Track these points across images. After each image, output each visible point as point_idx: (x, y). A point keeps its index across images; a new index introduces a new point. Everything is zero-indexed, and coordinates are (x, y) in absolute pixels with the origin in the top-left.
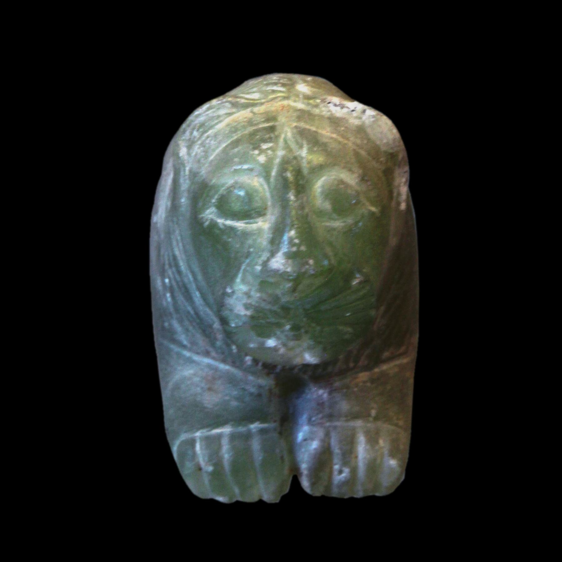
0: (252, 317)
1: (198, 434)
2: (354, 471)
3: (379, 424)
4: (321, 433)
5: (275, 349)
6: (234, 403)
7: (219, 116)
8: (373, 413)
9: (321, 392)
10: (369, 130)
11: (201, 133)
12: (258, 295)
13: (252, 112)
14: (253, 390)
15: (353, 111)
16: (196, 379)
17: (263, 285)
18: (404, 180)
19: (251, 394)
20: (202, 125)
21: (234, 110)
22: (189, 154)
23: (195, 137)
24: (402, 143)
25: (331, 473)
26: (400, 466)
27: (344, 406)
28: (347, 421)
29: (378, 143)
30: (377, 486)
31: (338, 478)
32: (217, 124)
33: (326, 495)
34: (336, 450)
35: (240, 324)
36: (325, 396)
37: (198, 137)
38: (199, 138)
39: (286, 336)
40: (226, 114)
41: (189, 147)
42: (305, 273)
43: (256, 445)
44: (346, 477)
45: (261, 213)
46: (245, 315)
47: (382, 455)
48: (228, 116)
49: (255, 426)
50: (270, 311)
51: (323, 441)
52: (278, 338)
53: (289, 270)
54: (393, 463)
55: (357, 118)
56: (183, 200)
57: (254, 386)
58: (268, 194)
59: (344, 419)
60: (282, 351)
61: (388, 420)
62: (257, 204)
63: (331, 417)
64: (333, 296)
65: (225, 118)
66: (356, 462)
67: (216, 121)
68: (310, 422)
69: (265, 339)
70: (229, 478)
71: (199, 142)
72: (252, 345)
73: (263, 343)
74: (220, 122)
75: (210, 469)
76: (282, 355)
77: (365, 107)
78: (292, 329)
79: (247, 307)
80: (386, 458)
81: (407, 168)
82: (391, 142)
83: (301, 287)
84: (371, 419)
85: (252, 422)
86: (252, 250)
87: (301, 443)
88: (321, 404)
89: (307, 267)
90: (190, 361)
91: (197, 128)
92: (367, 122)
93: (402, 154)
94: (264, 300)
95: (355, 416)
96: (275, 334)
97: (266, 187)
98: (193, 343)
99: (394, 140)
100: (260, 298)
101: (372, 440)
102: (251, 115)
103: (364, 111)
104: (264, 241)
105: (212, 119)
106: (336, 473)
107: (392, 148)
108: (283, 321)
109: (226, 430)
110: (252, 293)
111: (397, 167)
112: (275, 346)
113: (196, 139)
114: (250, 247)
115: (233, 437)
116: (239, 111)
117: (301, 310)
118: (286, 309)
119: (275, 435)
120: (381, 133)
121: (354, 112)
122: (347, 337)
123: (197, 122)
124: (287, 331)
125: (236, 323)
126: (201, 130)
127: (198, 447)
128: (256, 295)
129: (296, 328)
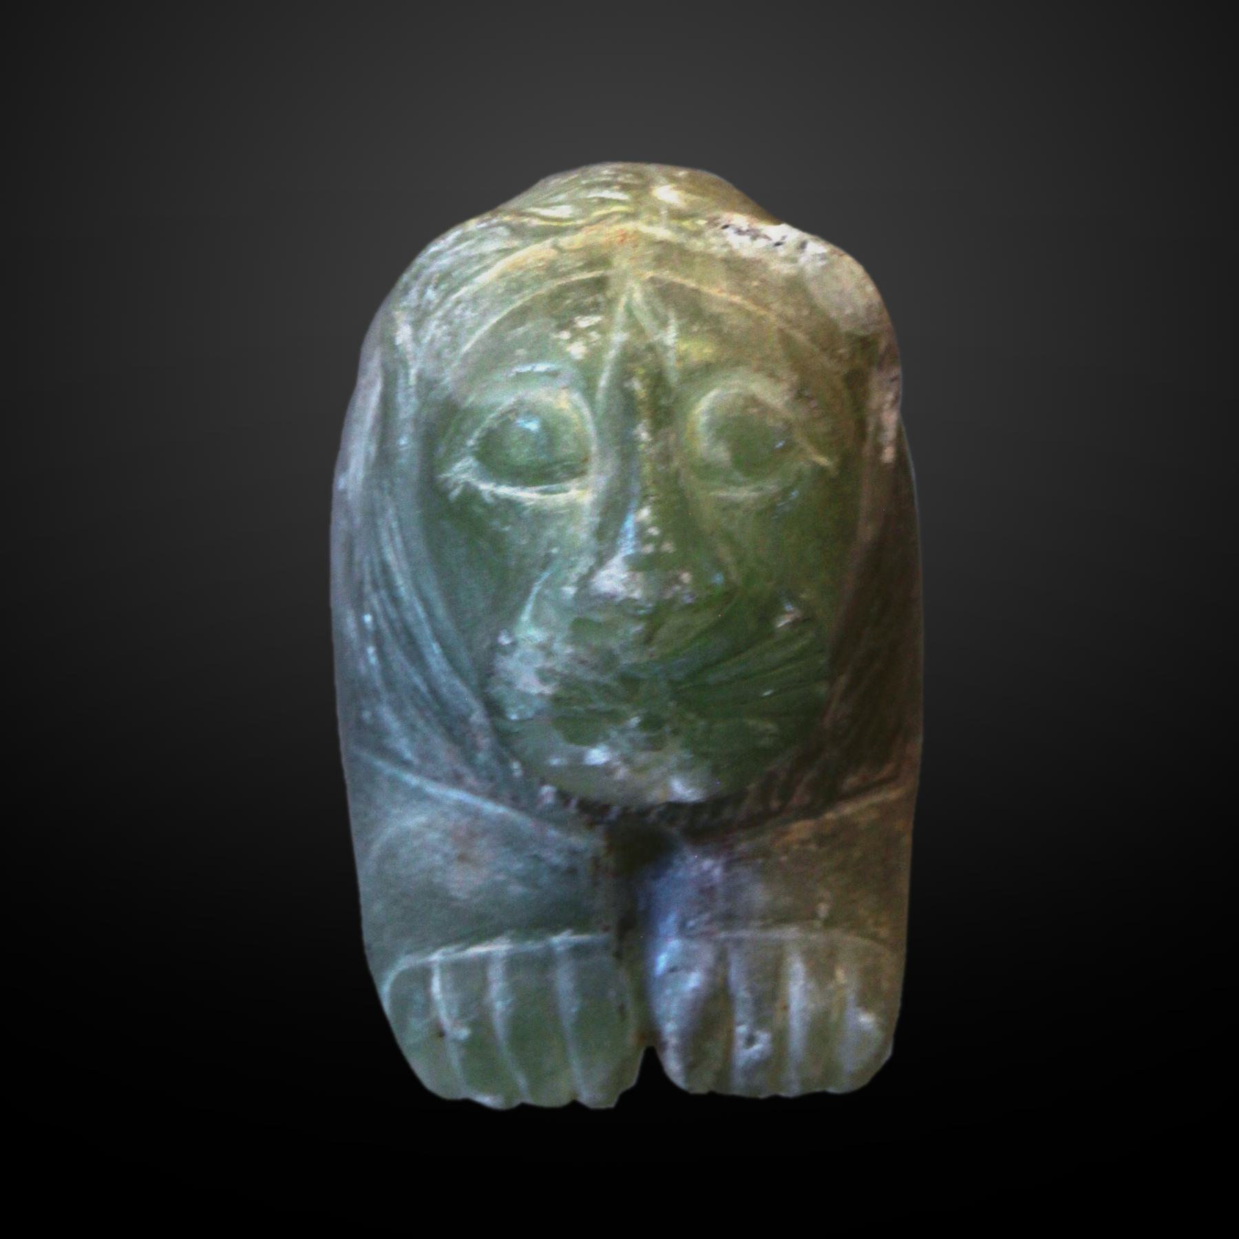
1: (436, 957)
2: (780, 1038)
3: (836, 934)
4: (707, 955)
5: (606, 770)
6: (516, 889)
7: (482, 257)
8: (823, 909)
9: (707, 864)
10: (813, 287)
11: (442, 294)
12: (569, 650)
13: (555, 247)
14: (557, 860)
15: (778, 244)
16: (433, 836)
17: (580, 628)
18: (890, 396)
19: (554, 869)
20: (446, 275)
21: (516, 243)
22: (416, 339)
23: (429, 302)
25: (730, 1042)
26: (883, 1028)
27: (759, 895)
28: (765, 927)
29: (834, 314)
30: (831, 1071)
31: (745, 1054)
32: (478, 273)
33: (719, 1091)
34: (742, 992)
35: (530, 714)
36: (717, 872)
37: (437, 301)
38: (440, 305)
39: (631, 741)
40: (499, 251)
41: (418, 325)
42: (672, 602)
43: (564, 980)
44: (762, 1052)
45: (575, 470)
46: (541, 695)
47: (843, 1004)
48: (503, 257)
49: (561, 940)
50: (596, 685)
51: (711, 972)
52: (613, 746)
53: (637, 594)
54: (866, 1020)
55: (786, 259)
56: (403, 441)
57: (560, 851)
58: (590, 429)
59: (759, 923)
60: (622, 773)
62: (567, 449)
63: (729, 919)
64: (735, 652)
65: (497, 260)
66: (785, 1019)
67: (476, 268)
68: (683, 930)
69: (584, 748)
70: (506, 1054)
71: (440, 313)
72: (555, 762)
73: (580, 757)
74: (486, 268)
75: (464, 1033)
76: (623, 783)
78: (644, 725)
79: (544, 676)
80: (851, 1009)
82: (862, 313)
83: (663, 633)
84: (818, 924)
85: (556, 931)
86: (554, 551)
87: (664, 976)
88: (707, 891)
89: (677, 588)
90: (419, 796)
91: (434, 281)
92: (810, 270)
94: (583, 662)
95: (782, 918)
96: (607, 737)
97: (586, 411)
98: (426, 756)
100: (574, 657)
101: (821, 969)
102: (552, 254)
105: (467, 261)
106: (740, 1043)
107: (864, 327)
108: (624, 707)
109: (499, 948)
110: (557, 646)
112: (607, 763)
113: (431, 307)
114: (551, 544)
115: (513, 964)
116: (526, 245)
117: (663, 684)
118: (630, 681)
119: (607, 959)
120: (841, 293)
121: (780, 248)
122: (765, 742)
123: (433, 269)
124: (634, 729)
125: (520, 712)
126: (443, 287)
127: (436, 986)
128: (565, 650)
129: (651, 723)
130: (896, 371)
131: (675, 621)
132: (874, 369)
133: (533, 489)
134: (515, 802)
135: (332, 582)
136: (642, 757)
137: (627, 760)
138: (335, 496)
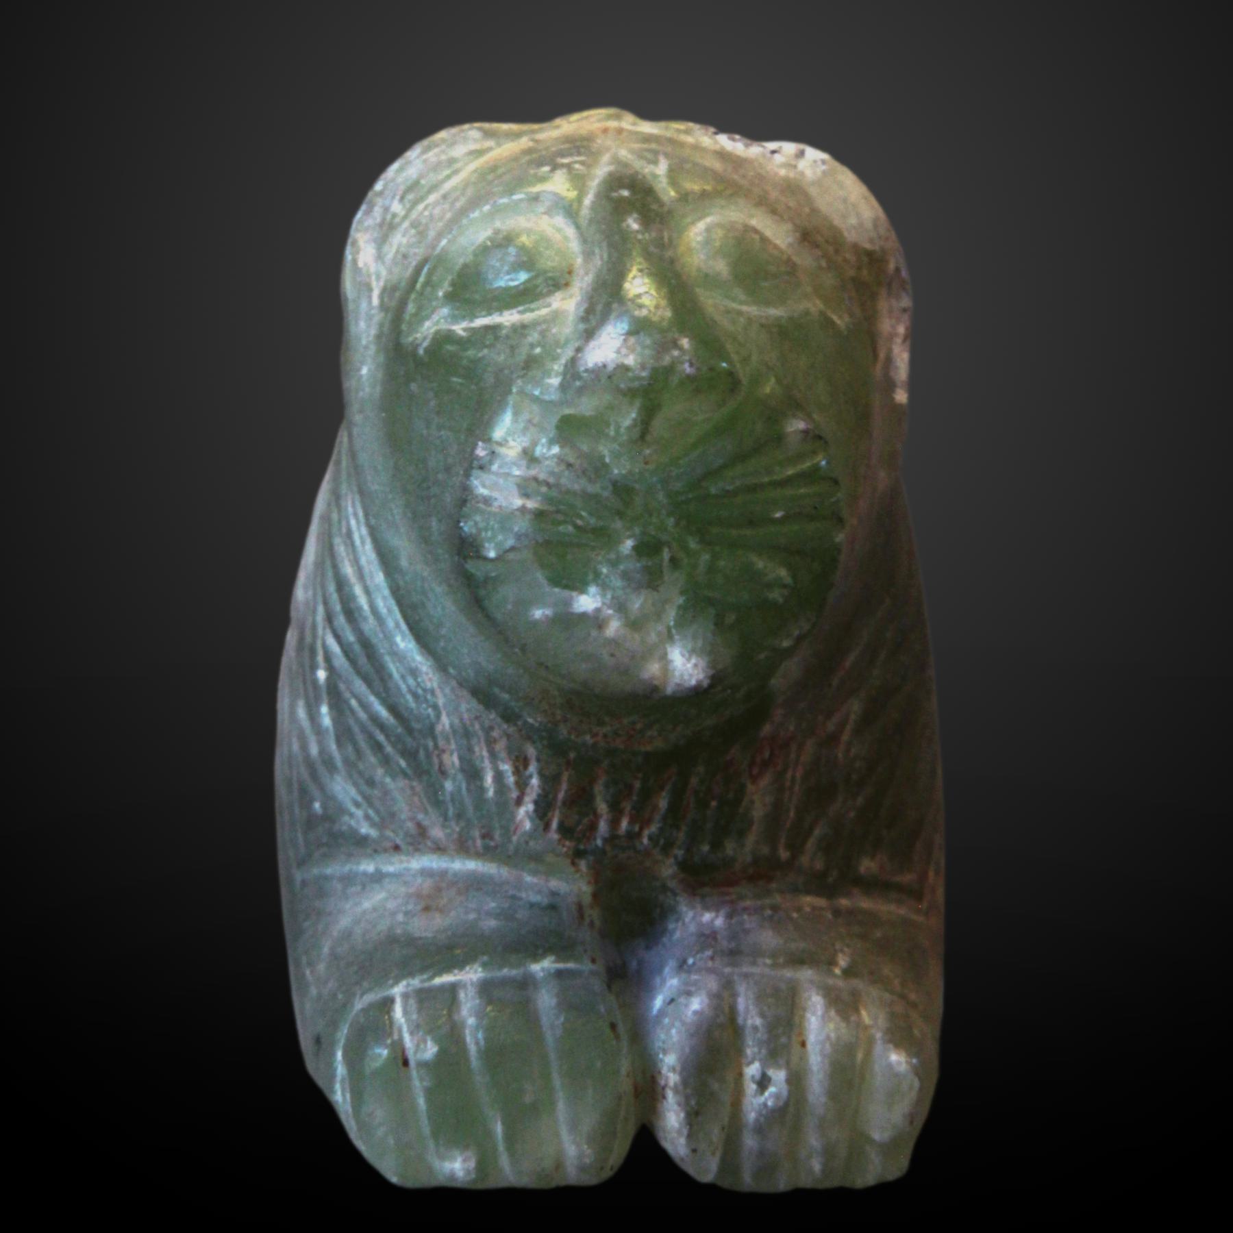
1: (398, 990)
2: (796, 1080)
3: (857, 983)
4: (712, 984)
5: (595, 621)
6: (491, 923)
7: (452, 161)
8: (843, 961)
9: (707, 917)
10: (813, 191)
11: (408, 206)
12: (556, 450)
13: (533, 140)
14: (535, 898)
16: (391, 905)
17: (568, 429)
18: (901, 330)
19: (532, 905)
20: (414, 186)
21: (490, 143)
23: (394, 215)
25: (739, 1092)
26: (918, 1072)
27: (768, 938)
28: (775, 966)
29: (837, 222)
30: (858, 1141)
31: (755, 1103)
32: (448, 177)
33: (726, 1183)
34: (751, 1017)
35: (510, 542)
36: (719, 922)
37: (403, 213)
38: (405, 217)
39: (625, 576)
40: (471, 153)
41: (381, 241)
42: (670, 370)
43: (546, 1000)
44: (777, 1096)
45: (558, 282)
46: (523, 509)
47: (871, 1042)
48: (477, 158)
49: (542, 967)
50: (587, 496)
51: (716, 997)
52: (604, 587)
53: (630, 360)
54: (897, 1058)
55: (787, 165)
56: (364, 371)
57: (539, 892)
58: (575, 246)
59: (768, 961)
60: (614, 627)
62: (549, 261)
63: (733, 955)
64: (740, 457)
65: (466, 164)
66: (803, 1058)
67: (447, 172)
68: (682, 966)
69: (574, 594)
70: (480, 1080)
71: (406, 224)
72: (538, 613)
73: (568, 603)
74: (456, 172)
75: (431, 1050)
76: (614, 642)
77: (801, 146)
78: (640, 550)
79: (525, 488)
80: (879, 1047)
82: (869, 225)
83: (659, 426)
84: (837, 971)
85: (536, 958)
86: (538, 350)
87: (657, 1016)
88: (707, 938)
89: (676, 353)
90: (378, 877)
91: (400, 192)
92: (809, 173)
94: (569, 465)
95: (797, 960)
96: (597, 575)
97: (571, 232)
98: (386, 819)
99: (876, 222)
100: (560, 459)
101: (842, 1004)
102: (531, 144)
103: (801, 154)
105: (436, 167)
106: (751, 1087)
107: (871, 241)
108: (618, 524)
109: (472, 975)
110: (539, 451)
112: (598, 610)
113: (397, 220)
114: (532, 346)
115: (485, 988)
116: (499, 145)
117: (661, 496)
118: (622, 490)
119: (597, 985)
120: (845, 200)
121: (776, 156)
122: (776, 595)
123: (400, 180)
124: (627, 557)
125: (498, 546)
126: (410, 197)
127: (398, 1012)
128: (550, 451)
129: (647, 548)
130: (906, 302)
131: (673, 408)
132: (883, 292)
134: (488, 853)
137: (621, 607)
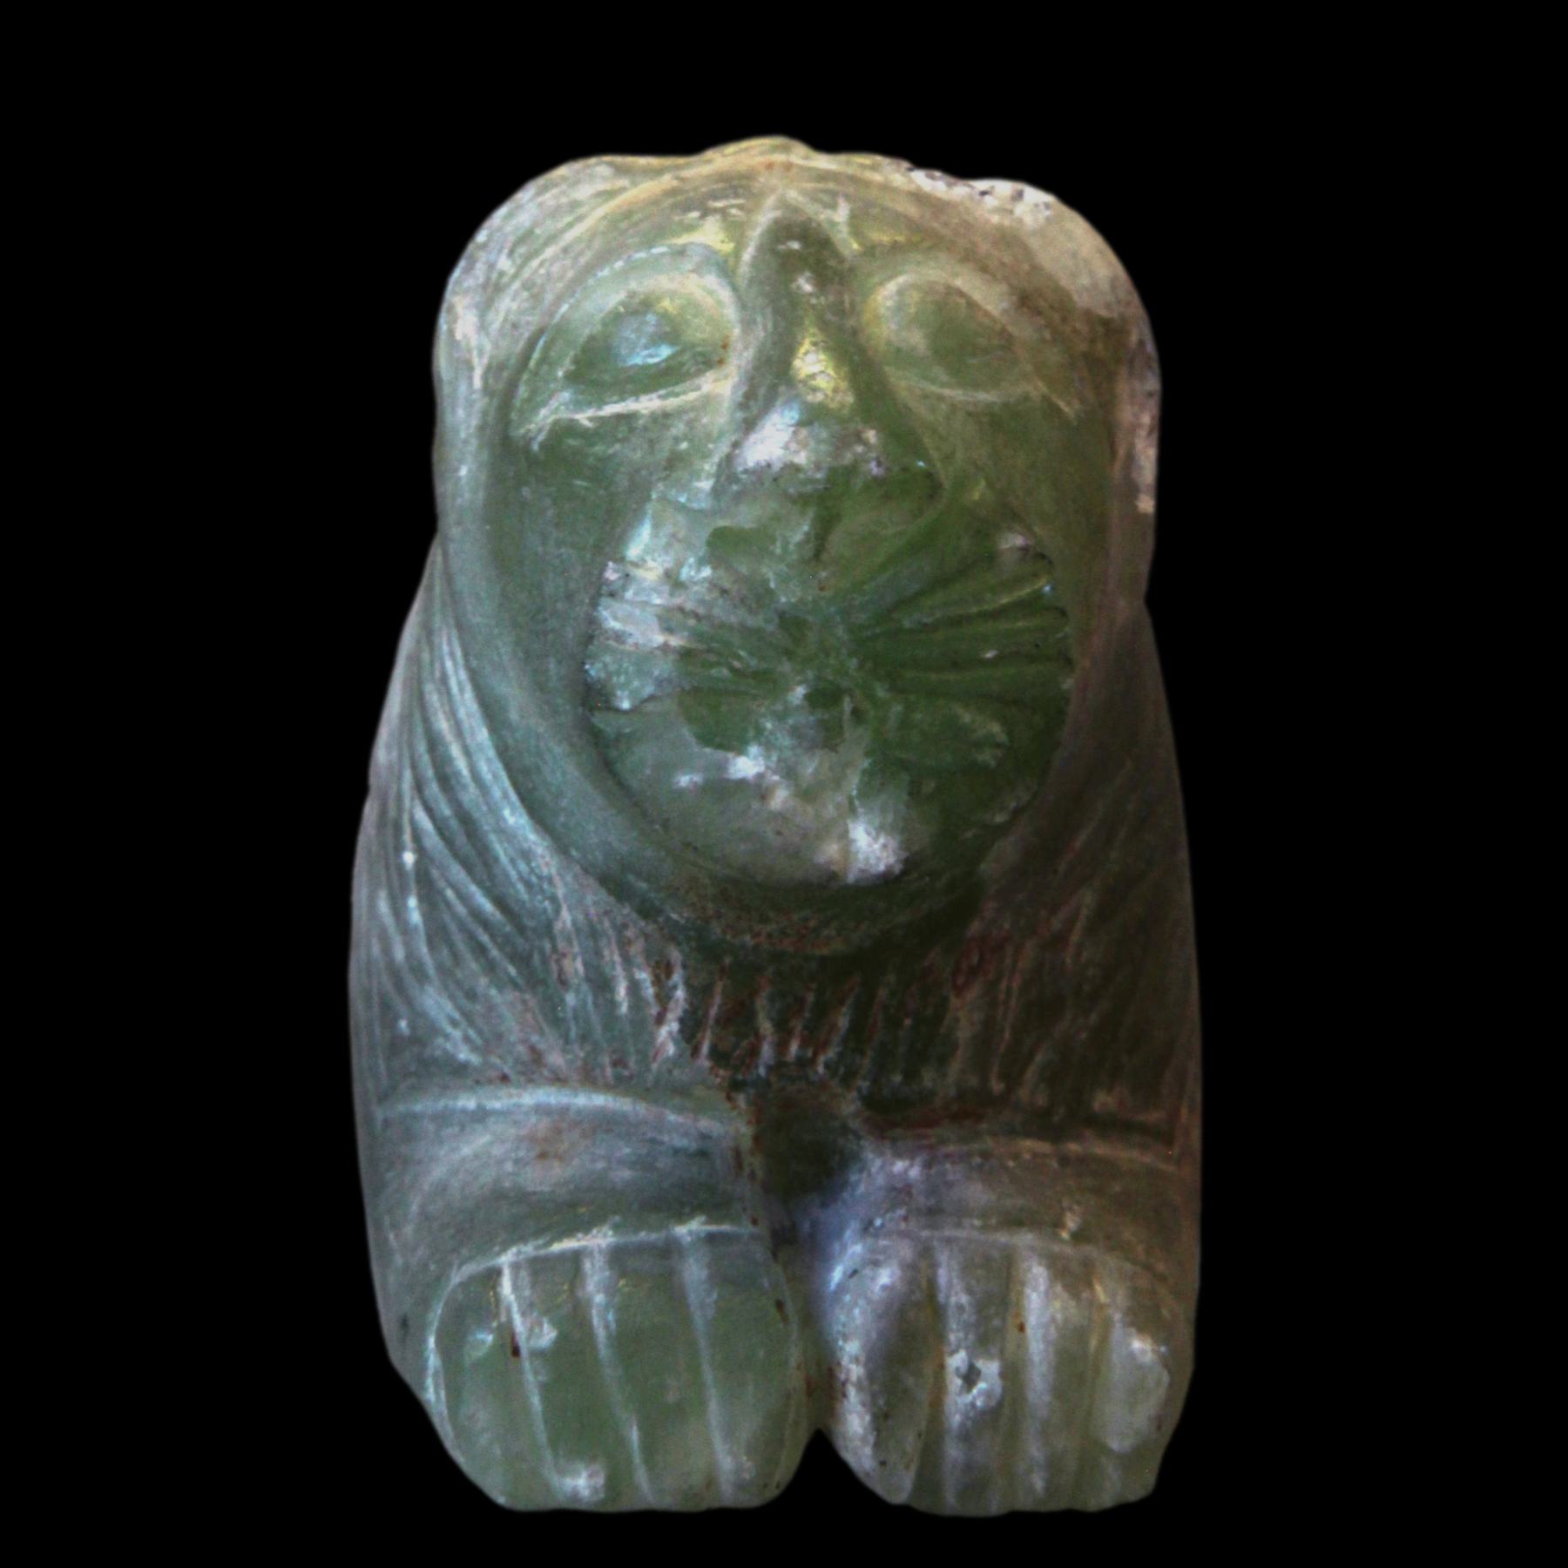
0: (686, 655)
1: (506, 1259)
2: (1013, 1374)
3: (1090, 1250)
4: (906, 1251)
5: (757, 789)
6: (625, 1174)
7: (575, 205)
8: (1072, 1222)
9: (899, 1166)
10: (1034, 243)
11: (519, 261)
12: (707, 572)
13: (677, 178)
14: (680, 1142)
16: (497, 1151)
17: (723, 546)
19: (676, 1151)
20: (526, 237)
21: (623, 182)
22: (483, 327)
23: (502, 274)
24: (1136, 300)
25: (939, 1389)
26: (1167, 1363)
27: (977, 1193)
28: (985, 1228)
29: (1064, 282)
30: (1091, 1452)
31: (960, 1403)
32: (570, 225)
33: (923, 1505)
34: (955, 1293)
35: (649, 690)
36: (915, 1172)
37: (512, 271)
38: (516, 276)
39: (795, 732)
40: (599, 194)
41: (485, 307)
42: (852, 470)
43: (694, 1272)
44: (988, 1394)
45: (710, 359)
46: (665, 648)
47: (1107, 1325)
48: (606, 200)
49: (689, 1230)
50: (746, 631)
51: (910, 1268)
52: (768, 746)
53: (802, 458)
54: (1141, 1346)
55: (1001, 210)
56: (463, 471)
57: (686, 1134)
58: (731, 313)
59: (977, 1222)
60: (781, 798)
61: (1113, 1244)
62: (698, 332)
63: (933, 1214)
64: (941, 582)
65: (593, 209)
66: (1022, 1345)
67: (568, 219)
68: (867, 1228)
69: (730, 755)
70: (610, 1373)
71: (516, 285)
72: (684, 780)
73: (722, 767)
74: (580, 219)
75: (547, 1335)
76: (781, 816)
77: (1019, 186)
78: (814, 699)
79: (667, 621)
80: (1117, 1332)
81: (1153, 383)
82: (1105, 286)
83: (838, 541)
84: (1065, 1235)
85: (682, 1218)
86: (684, 445)
87: (836, 1292)
88: (900, 1193)
89: (859, 449)
90: (481, 1116)
91: (509, 245)
92: (1029, 220)
93: (1140, 332)
94: (724, 592)
95: (1014, 1221)
96: (759, 731)
97: (726, 294)
98: (491, 1042)
100: (713, 584)
101: (1071, 1277)
102: (675, 183)
104: (721, 418)
105: (555, 213)
106: (955, 1383)
107: (1108, 306)
108: (786, 667)
109: (600, 1240)
110: (685, 573)
111: (1123, 371)
112: (760, 776)
113: (505, 280)
114: (677, 440)
115: (617, 1257)
116: (634, 184)
117: (840, 631)
118: (791, 623)
119: (760, 1252)
120: (1075, 255)
121: (987, 198)
122: (987, 757)
123: (508, 229)
124: (798, 708)
125: (633, 694)
126: (522, 250)
127: (506, 1287)
128: (699, 574)
129: (823, 697)
133: (654, 396)
135: (352, 1023)
136: (810, 767)
137: (789, 773)
138: (360, 1010)
